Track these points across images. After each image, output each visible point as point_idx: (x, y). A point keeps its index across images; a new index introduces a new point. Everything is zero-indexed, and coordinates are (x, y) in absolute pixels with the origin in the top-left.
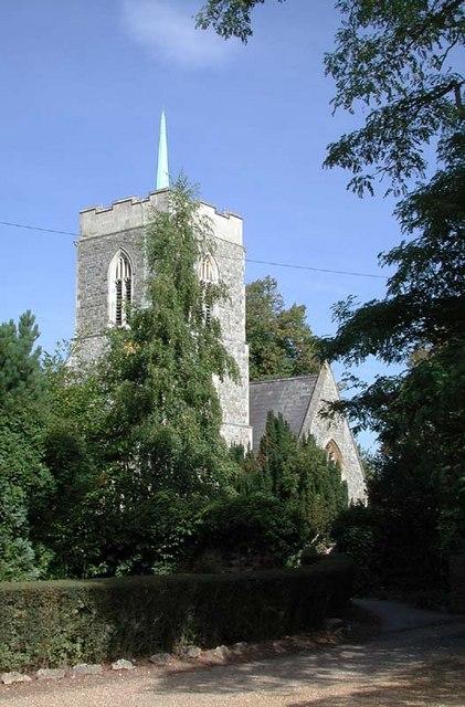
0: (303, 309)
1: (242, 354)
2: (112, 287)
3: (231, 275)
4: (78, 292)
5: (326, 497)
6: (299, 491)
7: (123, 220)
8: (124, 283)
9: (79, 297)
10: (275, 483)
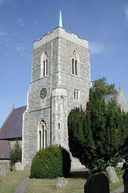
0: (114, 85)
1: (90, 85)
2: (42, 63)
3: (84, 58)
4: (32, 67)
5: (122, 131)
6: (106, 127)
7: (45, 41)
8: (46, 61)
9: (33, 69)
10: (93, 123)
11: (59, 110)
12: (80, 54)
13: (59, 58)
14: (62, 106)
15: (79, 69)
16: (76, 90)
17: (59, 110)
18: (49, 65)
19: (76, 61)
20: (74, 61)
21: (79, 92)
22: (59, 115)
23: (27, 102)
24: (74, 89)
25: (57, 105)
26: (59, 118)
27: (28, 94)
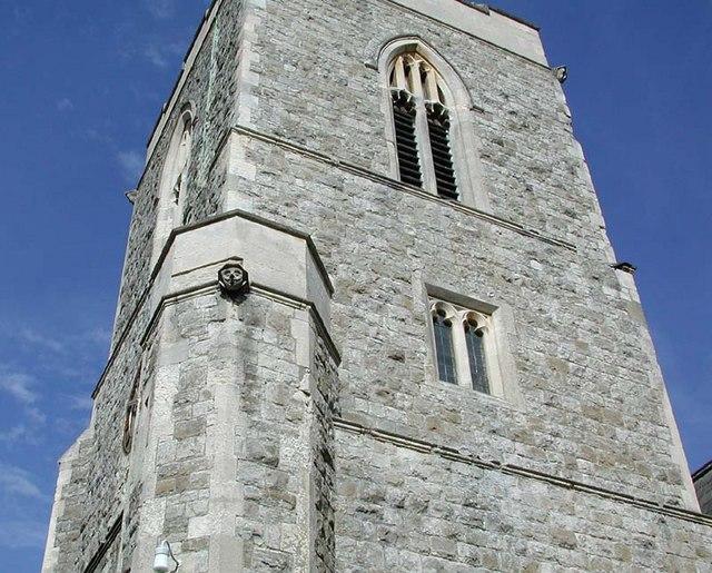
11: (191, 429)
12: (467, 74)
13: (248, 56)
14: (222, 386)
15: (473, 160)
16: (460, 302)
17: (191, 429)
18: (476, 512)
19: (438, 120)
20: (421, 112)
21: (494, 331)
22: (176, 480)
23: (51, 540)
24: (433, 292)
25: (166, 382)
26: (175, 525)
27: (63, 478)
